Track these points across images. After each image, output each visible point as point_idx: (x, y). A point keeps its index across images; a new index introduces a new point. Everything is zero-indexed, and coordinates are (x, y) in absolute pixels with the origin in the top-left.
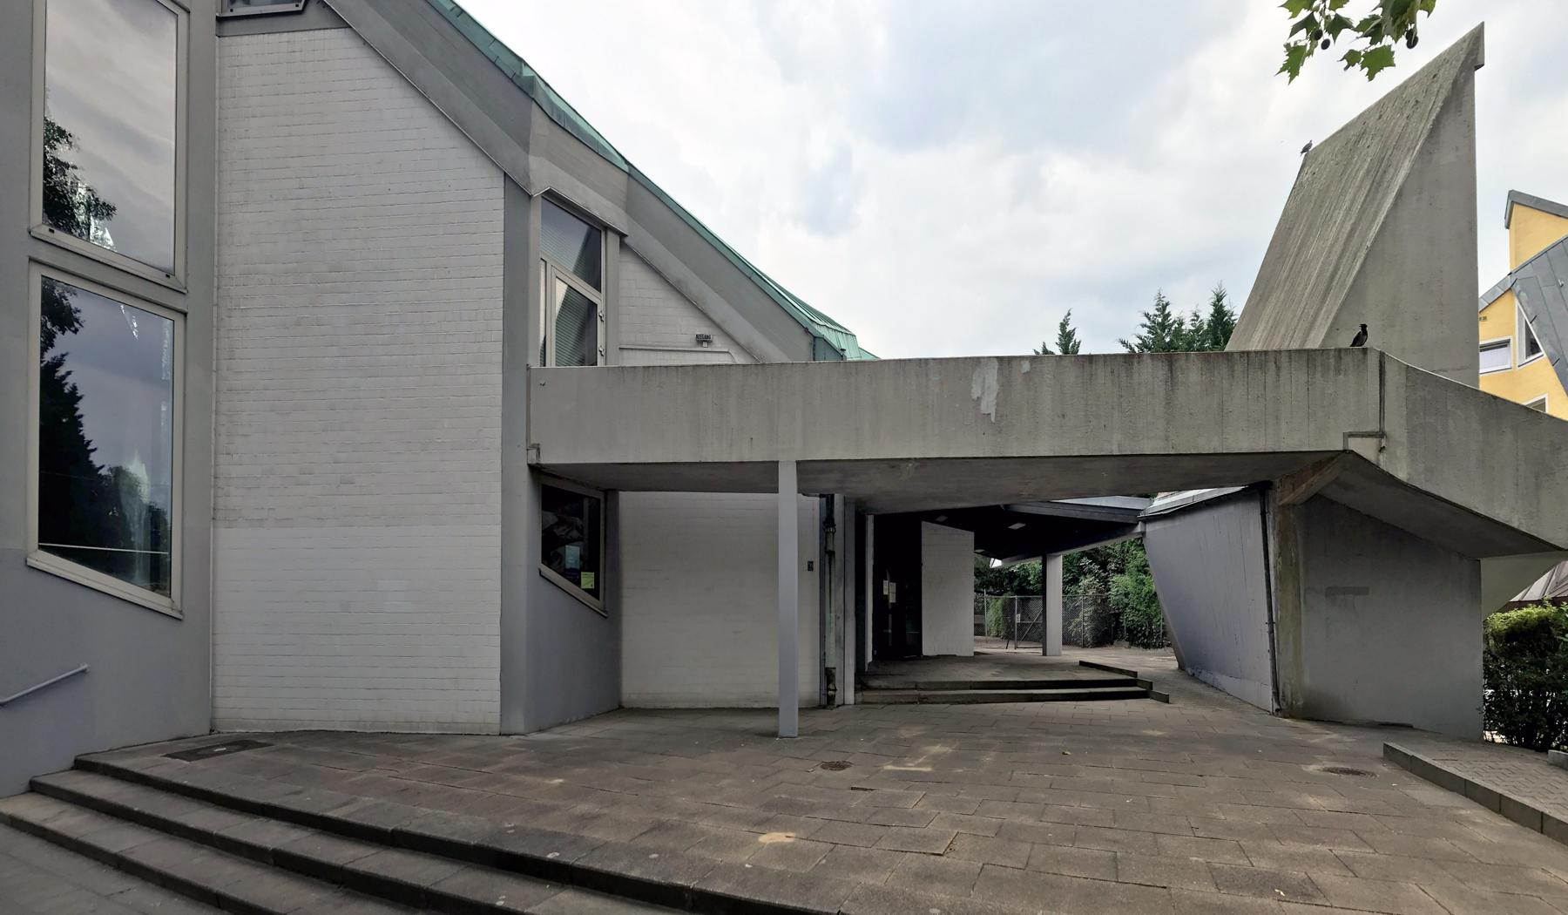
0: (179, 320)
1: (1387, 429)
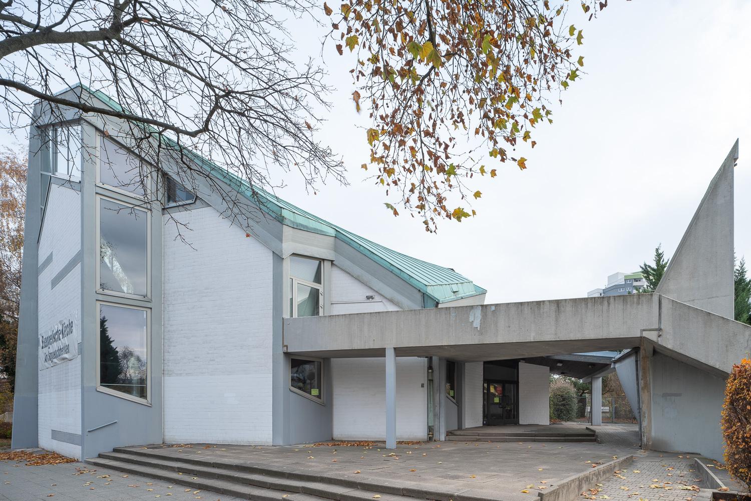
0: (149, 311)
1: (662, 327)
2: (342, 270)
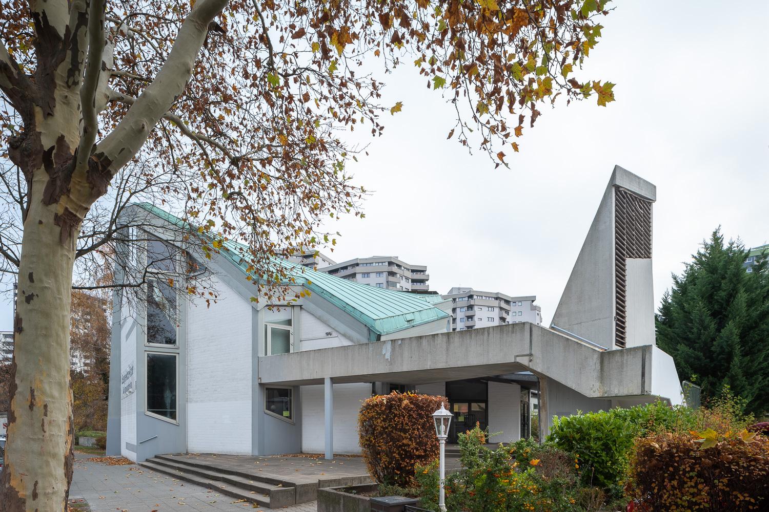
2: (308, 312)
